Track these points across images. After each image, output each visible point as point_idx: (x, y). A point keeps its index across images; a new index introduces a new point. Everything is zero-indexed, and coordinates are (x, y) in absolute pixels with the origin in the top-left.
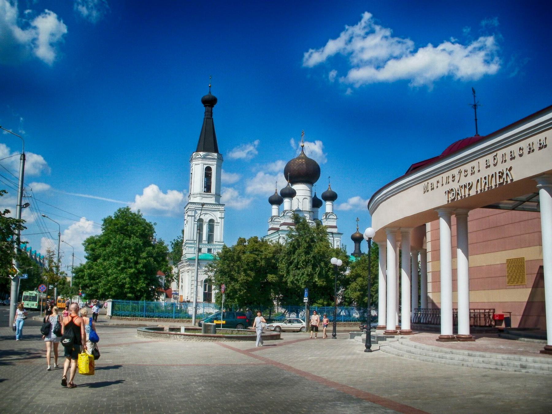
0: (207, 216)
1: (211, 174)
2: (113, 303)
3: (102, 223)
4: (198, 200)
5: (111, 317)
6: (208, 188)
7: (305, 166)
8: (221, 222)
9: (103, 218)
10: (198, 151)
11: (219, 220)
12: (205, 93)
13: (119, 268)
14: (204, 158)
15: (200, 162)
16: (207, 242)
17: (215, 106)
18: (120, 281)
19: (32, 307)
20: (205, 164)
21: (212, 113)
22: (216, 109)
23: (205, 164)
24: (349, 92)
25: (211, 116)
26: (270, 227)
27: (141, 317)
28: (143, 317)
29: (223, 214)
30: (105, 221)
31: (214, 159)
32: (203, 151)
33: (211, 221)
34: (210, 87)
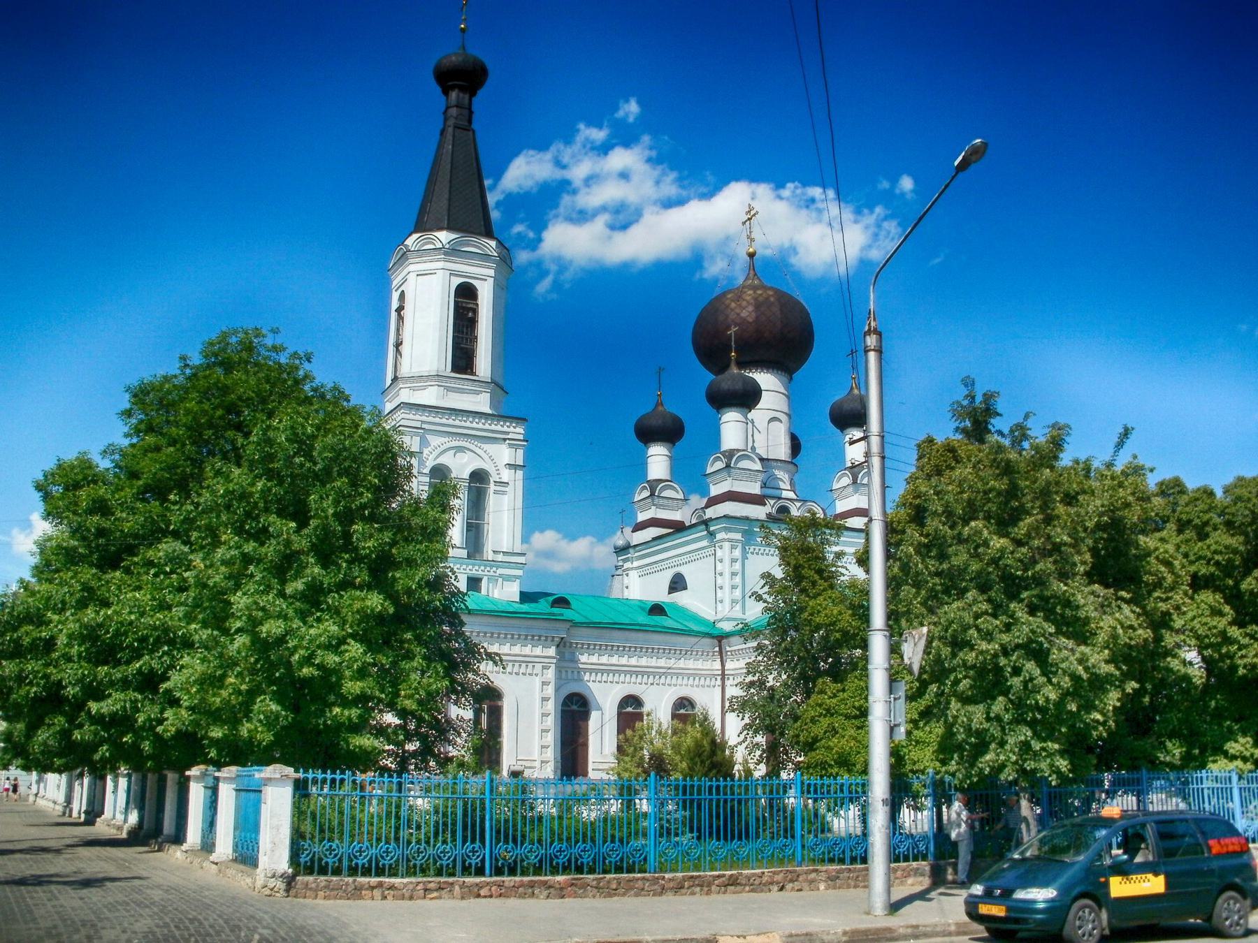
0: (464, 458)
1: (475, 311)
2: (300, 788)
3: (125, 402)
4: (430, 396)
5: (290, 881)
6: (463, 360)
7: (776, 309)
8: (516, 479)
9: (134, 382)
10: (422, 225)
11: (506, 475)
12: (448, 51)
13: (299, 585)
14: (452, 252)
15: (441, 264)
16: (464, 553)
17: (481, 93)
18: (308, 661)
19: (1231, 848)
20: (453, 274)
21: (471, 112)
22: (481, 99)
23: (453, 274)
24: (544, 285)
25: (470, 121)
26: (642, 517)
27: (466, 870)
28: (480, 872)
29: (520, 452)
30: (141, 395)
31: (485, 257)
32: (450, 228)
33: (479, 477)
34: (463, 30)
